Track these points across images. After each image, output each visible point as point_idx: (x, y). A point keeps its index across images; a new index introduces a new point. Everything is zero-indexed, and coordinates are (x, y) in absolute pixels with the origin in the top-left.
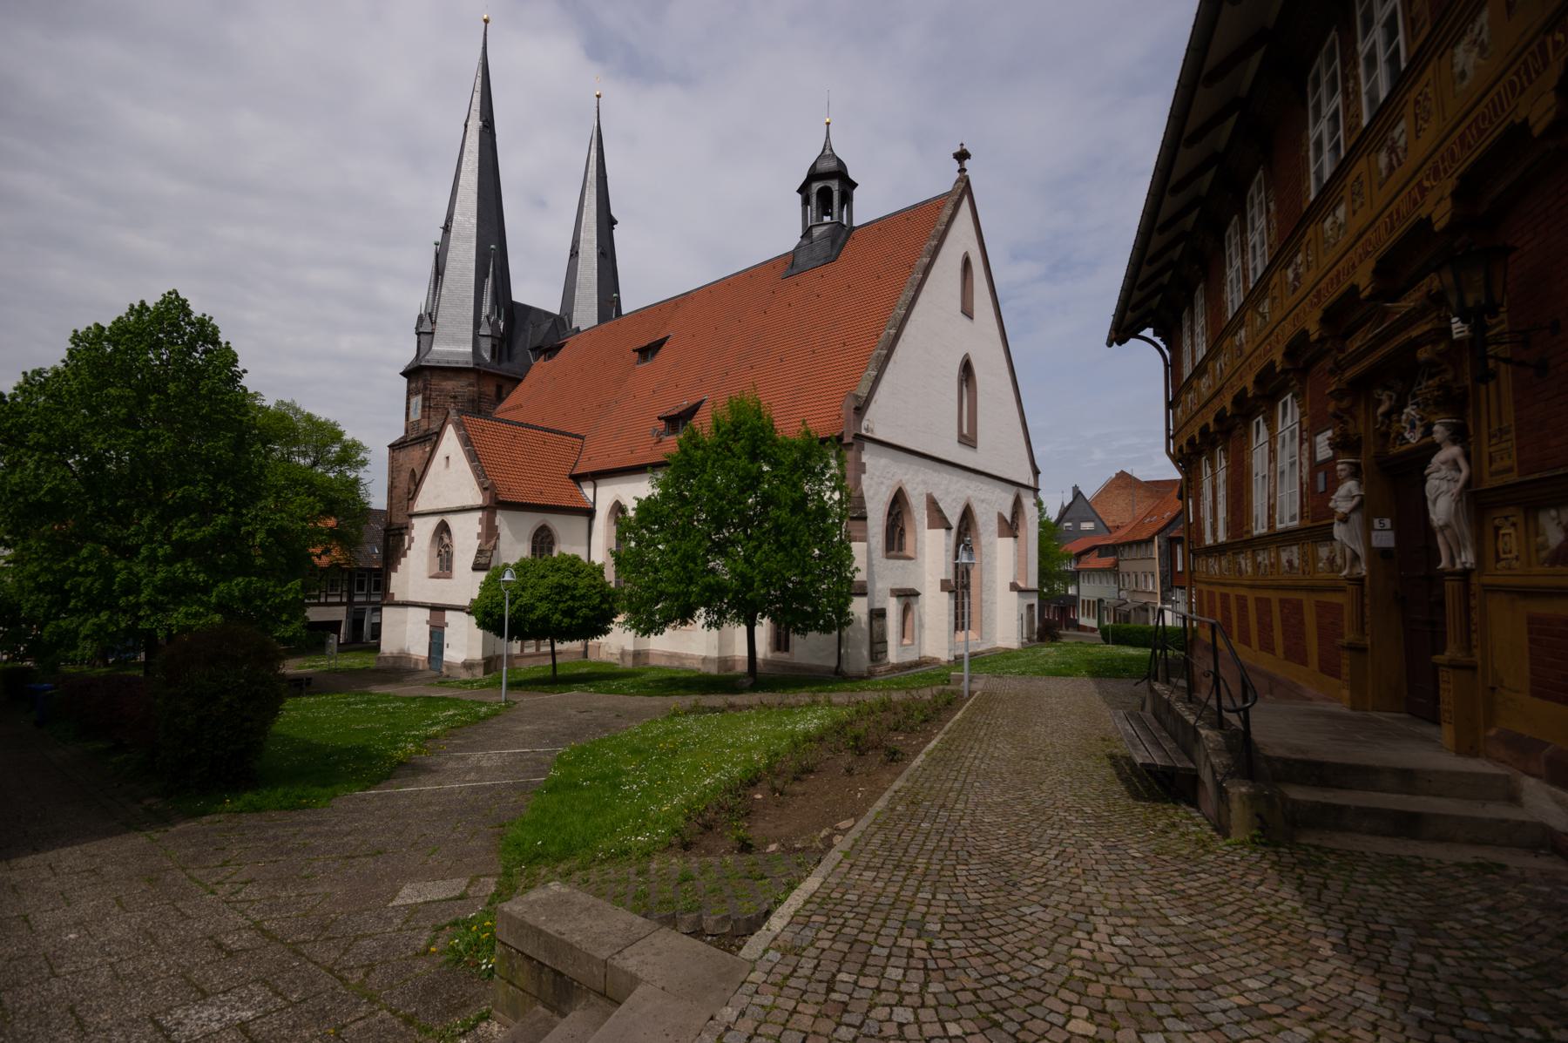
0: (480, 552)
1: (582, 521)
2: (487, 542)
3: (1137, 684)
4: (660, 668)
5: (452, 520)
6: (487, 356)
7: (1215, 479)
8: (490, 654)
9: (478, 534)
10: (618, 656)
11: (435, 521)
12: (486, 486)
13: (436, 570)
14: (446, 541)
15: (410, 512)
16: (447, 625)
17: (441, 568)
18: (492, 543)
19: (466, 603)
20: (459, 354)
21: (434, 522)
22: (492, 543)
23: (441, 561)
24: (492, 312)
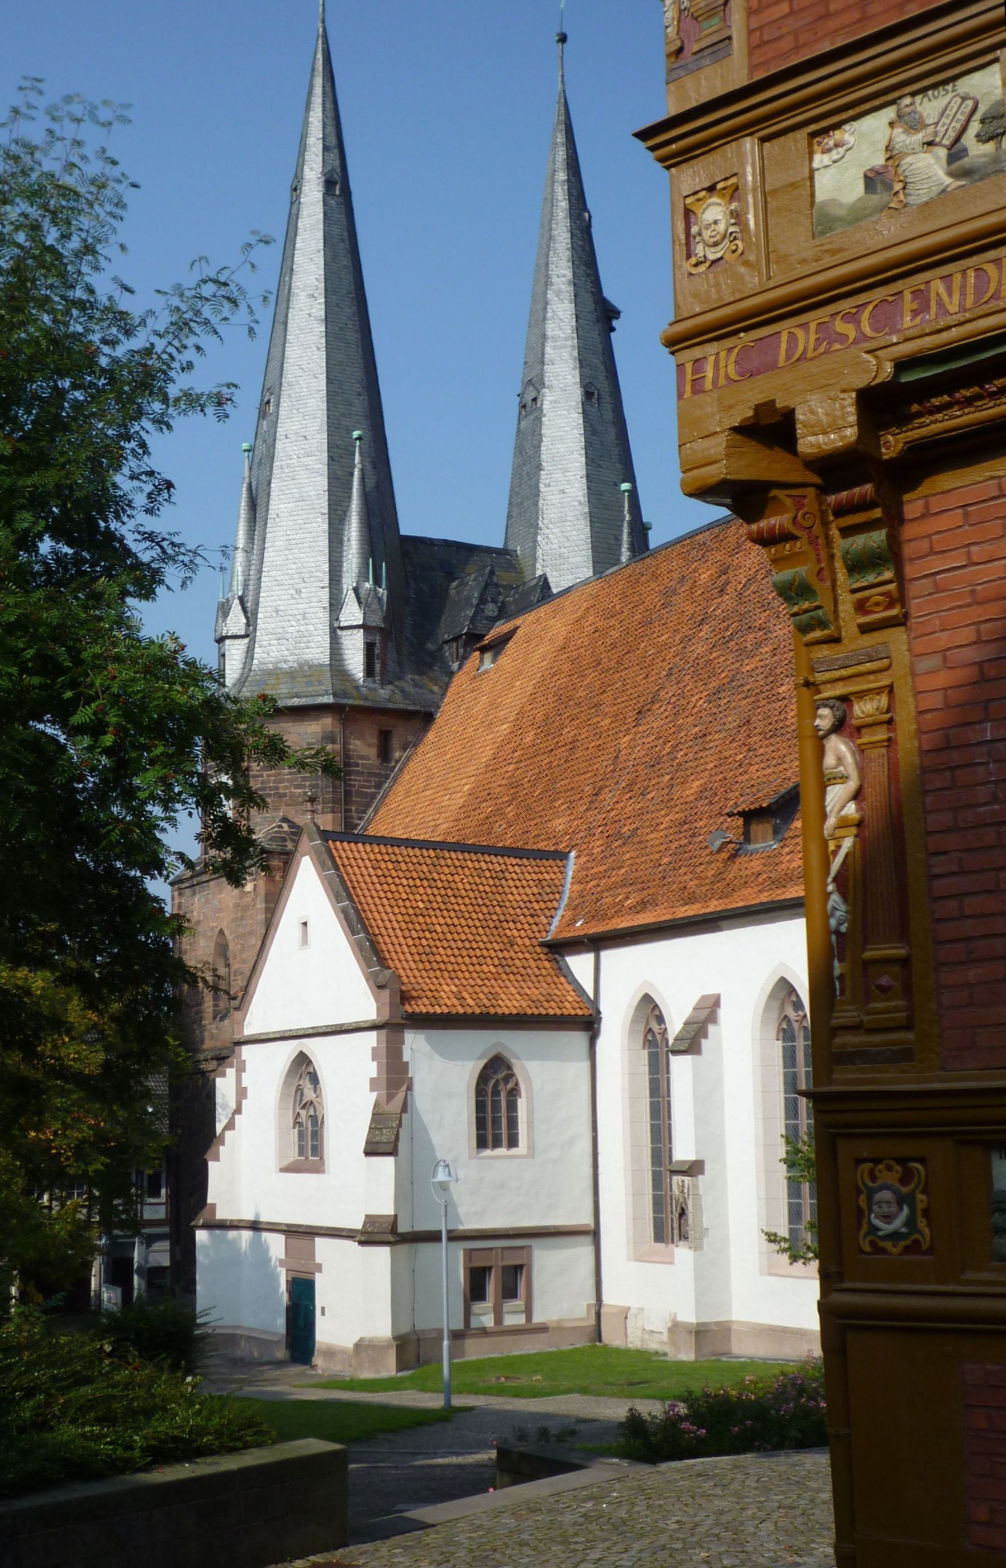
0: (378, 1118)
1: (578, 1039)
2: (390, 1097)
3: (136, 540)
4: (751, 1364)
5: (316, 1048)
6: (355, 661)
7: (245, 580)
8: (405, 1329)
9: (372, 1080)
10: (665, 1337)
11: (288, 1050)
12: (381, 980)
13: (293, 1155)
14: (309, 1094)
15: (237, 1037)
16: (319, 1268)
17: (301, 1151)
18: (401, 1095)
19: (358, 1224)
20: (808, 1108)
21: (286, 1052)
22: (401, 1095)
23: (301, 1136)
24: (363, 576)
